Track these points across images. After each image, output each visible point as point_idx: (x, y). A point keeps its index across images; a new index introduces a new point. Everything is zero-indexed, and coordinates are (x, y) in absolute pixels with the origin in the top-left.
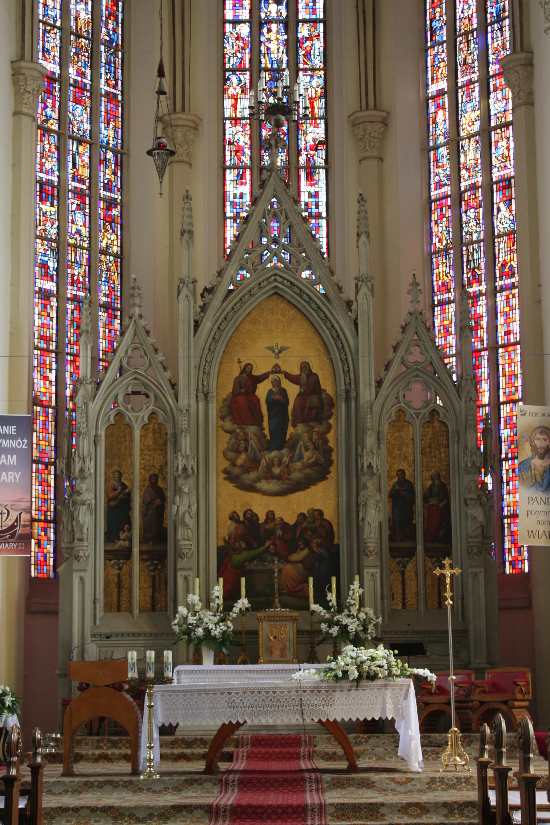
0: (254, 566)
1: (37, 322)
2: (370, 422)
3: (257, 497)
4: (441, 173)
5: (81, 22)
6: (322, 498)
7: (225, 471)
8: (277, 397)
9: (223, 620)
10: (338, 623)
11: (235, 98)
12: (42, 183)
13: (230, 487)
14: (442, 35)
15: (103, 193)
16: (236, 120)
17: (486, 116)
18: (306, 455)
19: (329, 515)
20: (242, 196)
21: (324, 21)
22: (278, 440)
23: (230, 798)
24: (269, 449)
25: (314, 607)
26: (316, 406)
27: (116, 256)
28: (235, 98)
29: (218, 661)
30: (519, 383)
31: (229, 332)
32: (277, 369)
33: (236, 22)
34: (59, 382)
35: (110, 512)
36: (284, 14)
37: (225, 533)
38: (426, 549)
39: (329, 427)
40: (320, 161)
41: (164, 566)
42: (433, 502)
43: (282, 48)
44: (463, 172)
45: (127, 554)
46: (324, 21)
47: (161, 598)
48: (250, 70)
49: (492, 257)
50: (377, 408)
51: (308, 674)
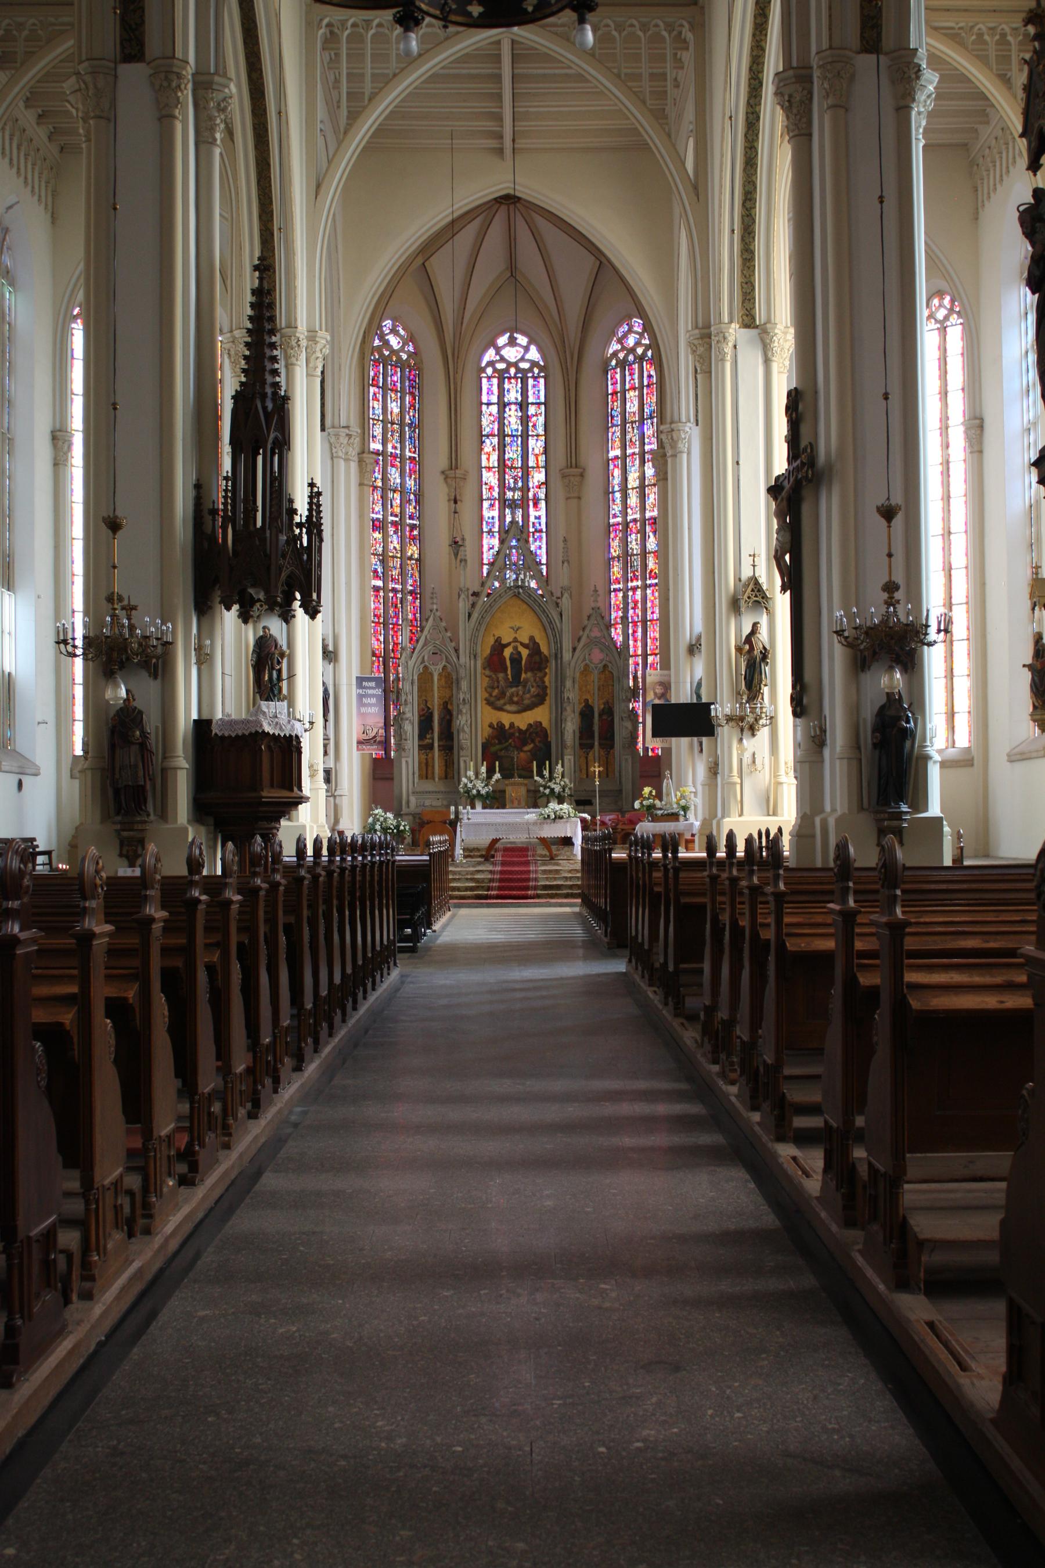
0: (502, 753)
1: (373, 606)
2: (568, 673)
3: (504, 714)
4: (616, 508)
5: (394, 416)
6: (541, 715)
7: (486, 699)
8: (516, 656)
9: (486, 785)
10: (549, 787)
11: (488, 454)
12: (373, 520)
13: (489, 708)
14: (618, 420)
15: (408, 521)
16: (489, 469)
17: (642, 477)
18: (532, 690)
19: (545, 724)
20: (493, 518)
21: (545, 404)
22: (516, 681)
23: (498, 868)
24: (511, 687)
25: (536, 778)
26: (538, 661)
27: (416, 560)
28: (488, 454)
29: (484, 808)
30: (658, 644)
31: (487, 619)
32: (515, 640)
33: (489, 404)
34: (386, 642)
35: (420, 722)
36: (520, 399)
37: (486, 735)
38: (600, 744)
39: (546, 674)
40: (542, 496)
41: (452, 753)
42: (604, 717)
43: (519, 422)
44: (629, 510)
45: (431, 747)
46: (545, 404)
47: (451, 772)
48: (498, 435)
49: (645, 565)
50: (573, 664)
51: (531, 815)
